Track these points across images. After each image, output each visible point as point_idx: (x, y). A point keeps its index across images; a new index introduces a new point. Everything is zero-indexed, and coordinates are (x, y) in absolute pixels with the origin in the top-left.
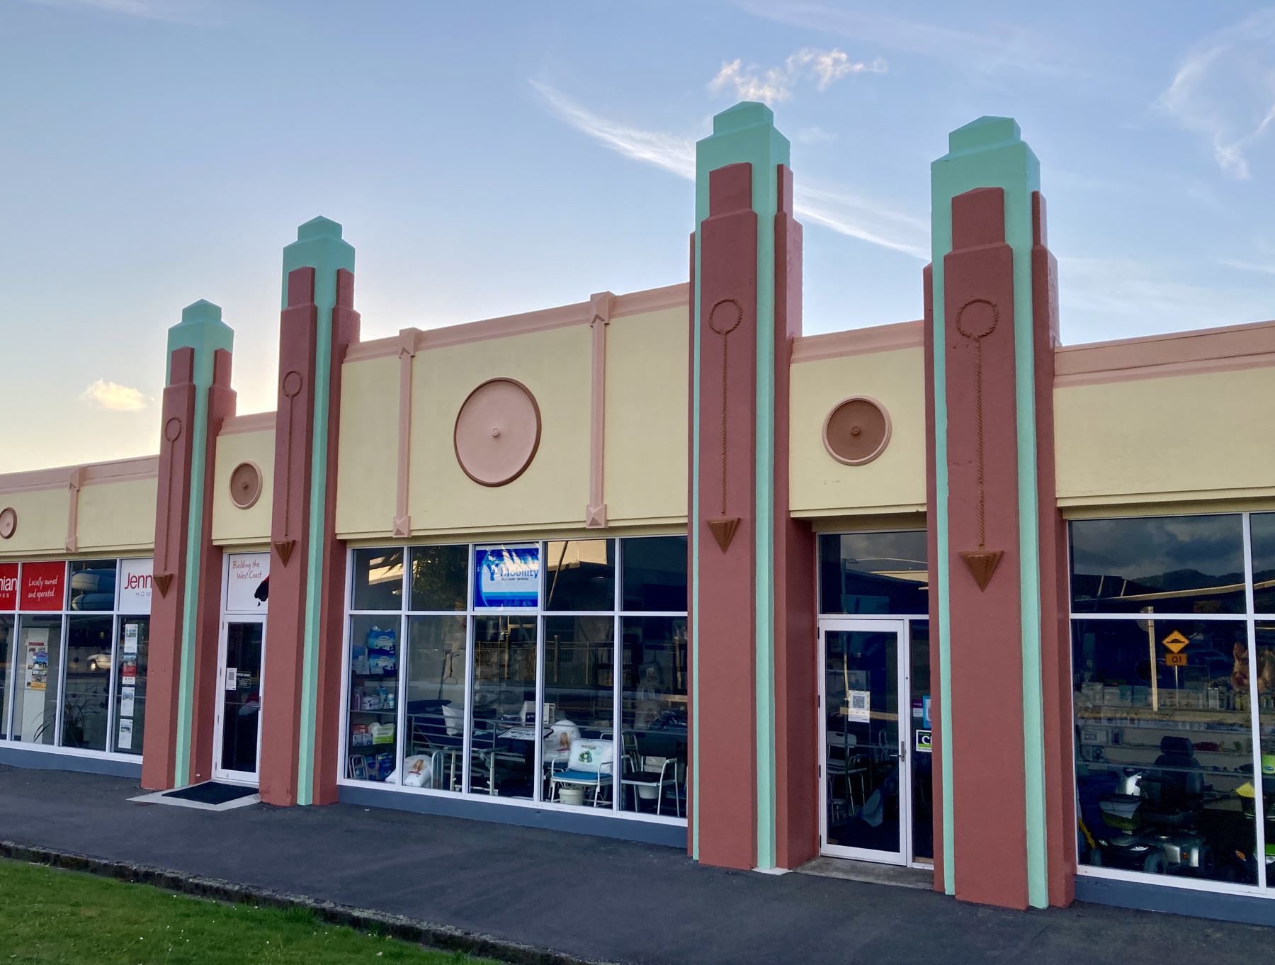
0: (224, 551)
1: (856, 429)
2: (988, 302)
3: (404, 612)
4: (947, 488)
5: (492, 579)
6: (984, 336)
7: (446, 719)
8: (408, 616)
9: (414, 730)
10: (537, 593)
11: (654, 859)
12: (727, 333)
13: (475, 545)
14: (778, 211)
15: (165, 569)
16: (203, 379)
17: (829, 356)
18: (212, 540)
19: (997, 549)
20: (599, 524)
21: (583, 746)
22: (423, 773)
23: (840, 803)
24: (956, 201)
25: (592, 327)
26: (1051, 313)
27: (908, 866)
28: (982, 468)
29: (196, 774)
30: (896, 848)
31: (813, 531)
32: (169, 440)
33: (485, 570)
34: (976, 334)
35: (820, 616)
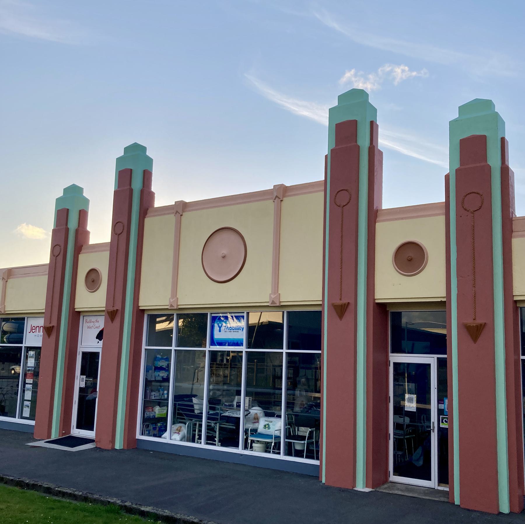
0: (81, 314)
1: (410, 257)
3: (173, 348)
5: (220, 331)
9: (178, 411)
10: (243, 339)
13: (211, 313)
15: (50, 323)
18: (139, 306)
20: (174, 307)
21: (266, 421)
22: (181, 433)
23: (400, 454)
27: (436, 489)
31: (387, 310)
32: (54, 256)
33: (216, 325)
35: (390, 354)
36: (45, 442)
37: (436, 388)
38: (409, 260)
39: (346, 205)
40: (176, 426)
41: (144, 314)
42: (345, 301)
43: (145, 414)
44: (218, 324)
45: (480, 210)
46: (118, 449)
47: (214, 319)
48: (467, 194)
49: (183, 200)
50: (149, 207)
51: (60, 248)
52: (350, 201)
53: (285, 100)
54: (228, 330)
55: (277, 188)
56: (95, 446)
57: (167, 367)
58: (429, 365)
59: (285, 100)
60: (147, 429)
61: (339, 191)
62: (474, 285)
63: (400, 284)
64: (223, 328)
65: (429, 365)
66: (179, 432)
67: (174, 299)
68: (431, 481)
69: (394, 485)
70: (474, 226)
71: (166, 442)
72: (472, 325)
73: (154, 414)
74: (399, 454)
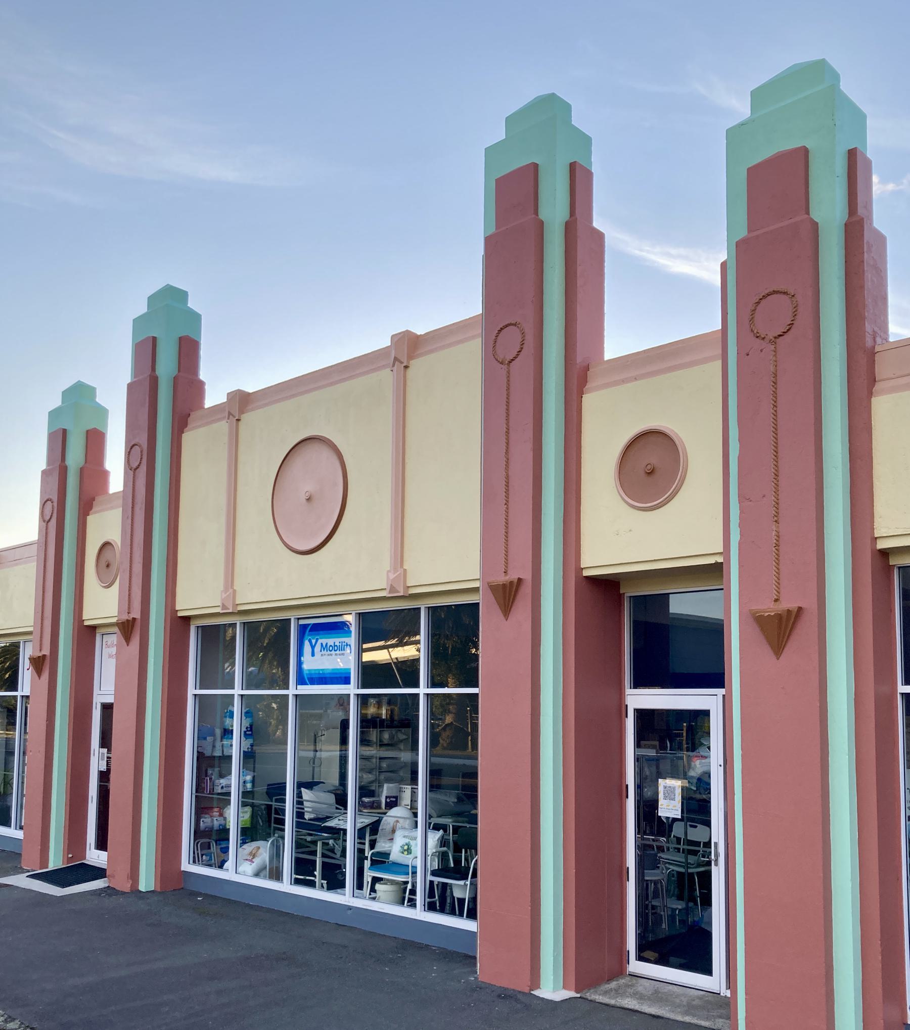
0: (97, 632)
1: (649, 467)
2: (785, 293)
3: (237, 691)
4: (738, 530)
5: (313, 655)
6: (780, 336)
7: (304, 802)
8: (242, 696)
9: (275, 814)
10: (350, 669)
11: (434, 971)
12: (510, 362)
13: (298, 619)
14: (571, 216)
15: (40, 650)
16: (75, 457)
17: (623, 381)
19: (793, 605)
20: (398, 592)
21: (404, 837)
22: (257, 861)
23: (680, 907)
24: (498, 181)
25: (392, 371)
26: (869, 301)
27: (722, 994)
28: (777, 504)
29: (68, 854)
30: (706, 969)
31: (621, 593)
32: (44, 521)
33: (307, 643)
34: (771, 336)
35: (629, 691)
36: (27, 877)
37: (720, 766)
38: (648, 473)
39: (515, 358)
40: (251, 846)
41: (190, 625)
42: (788, 603)
43: (201, 822)
44: (310, 641)
45: (789, 332)
46: (144, 891)
47: (302, 630)
48: (761, 297)
49: (240, 389)
50: (192, 411)
51: (53, 506)
52: (522, 348)
53: (648, 248)
54: (327, 651)
55: (396, 339)
56: (107, 885)
57: (249, 729)
58: (706, 713)
59: (648, 248)
60: (205, 852)
61: (502, 329)
62: (776, 518)
63: (630, 531)
64: (318, 648)
65: (706, 713)
66: (252, 859)
67: (228, 593)
68: (712, 976)
69: (634, 981)
70: (775, 375)
71: (228, 879)
72: (767, 614)
73: (223, 822)
74: (677, 908)
